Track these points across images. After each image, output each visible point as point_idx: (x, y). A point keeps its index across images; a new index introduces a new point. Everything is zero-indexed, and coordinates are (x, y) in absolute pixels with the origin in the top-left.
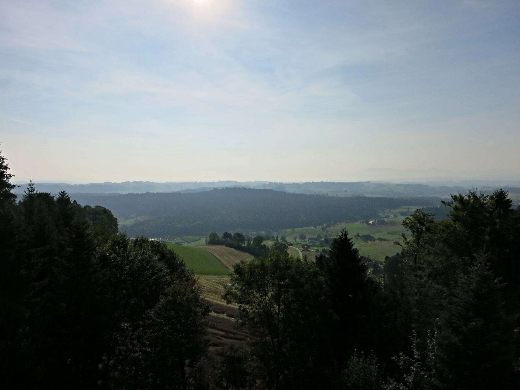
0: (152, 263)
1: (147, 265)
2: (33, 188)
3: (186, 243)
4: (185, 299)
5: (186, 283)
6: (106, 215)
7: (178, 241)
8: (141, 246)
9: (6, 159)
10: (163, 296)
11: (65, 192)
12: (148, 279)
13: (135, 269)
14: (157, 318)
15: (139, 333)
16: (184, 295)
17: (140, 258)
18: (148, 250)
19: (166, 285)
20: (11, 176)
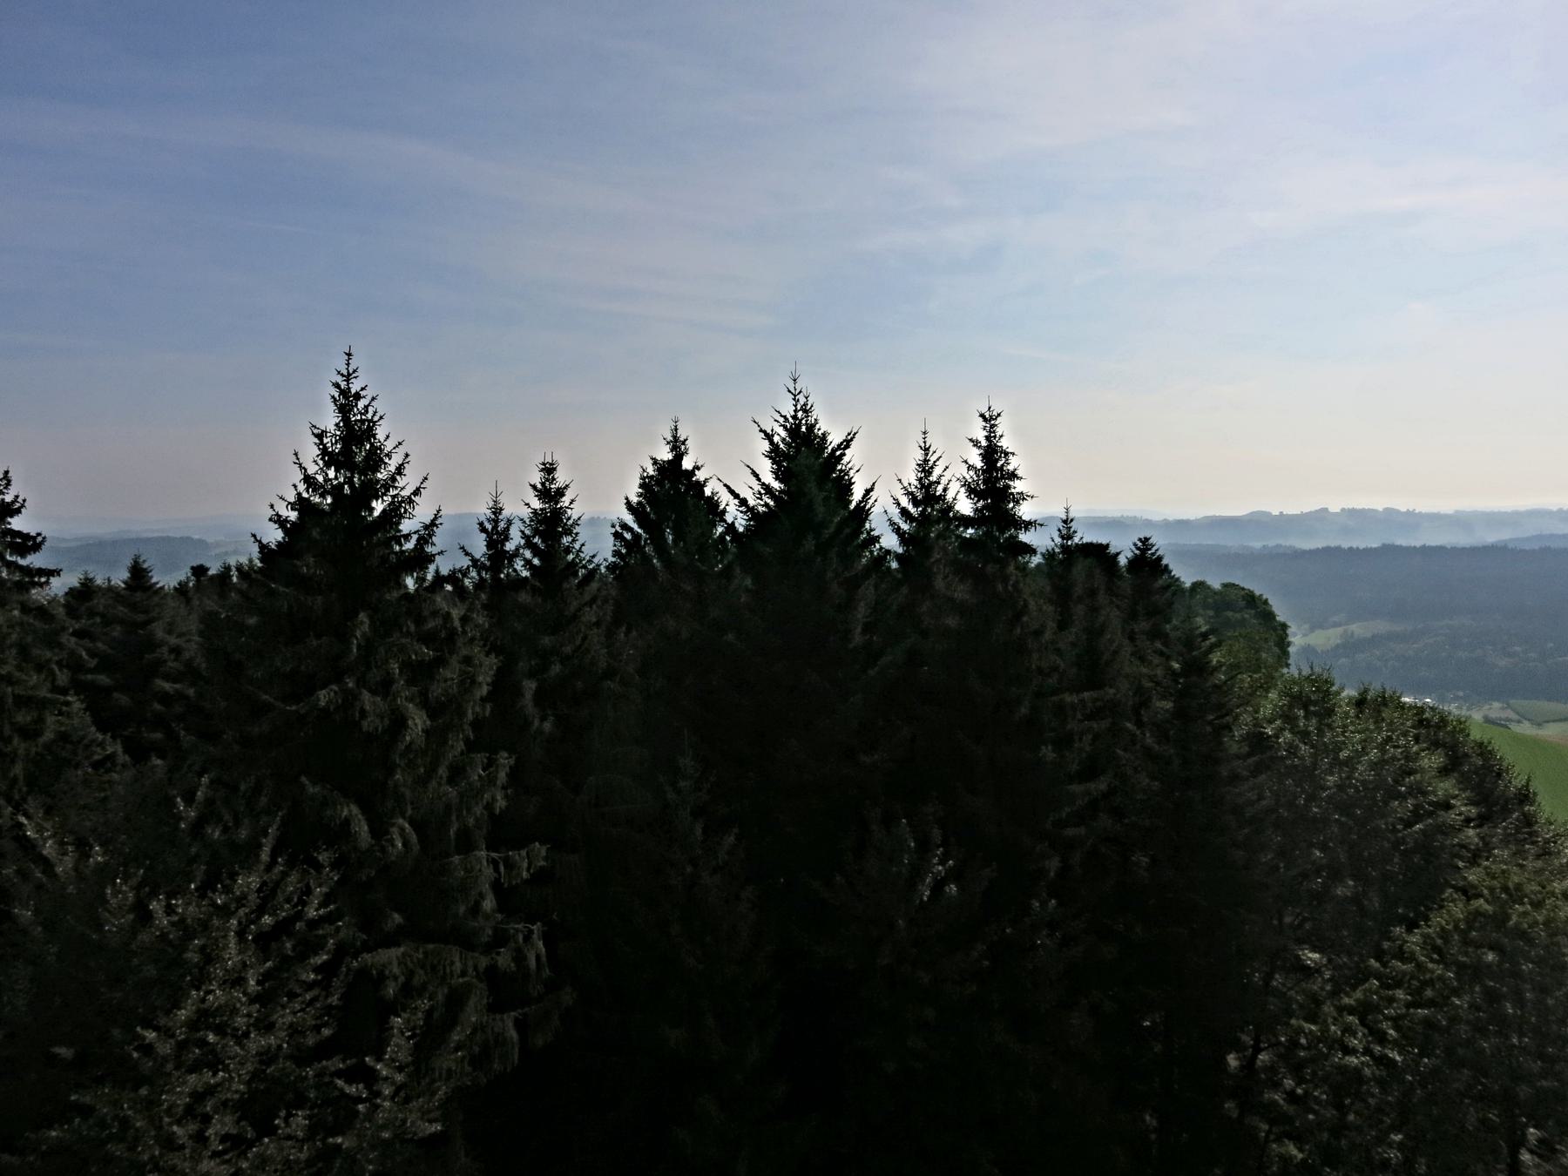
0: (1418, 776)
1: (1396, 782)
2: (1072, 530)
3: (1527, 724)
4: (1540, 919)
5: (1539, 864)
6: (1253, 612)
7: (1493, 715)
8: (1378, 720)
9: (1013, 454)
10: (1456, 893)
11: (1151, 541)
12: (1400, 827)
13: (1356, 788)
14: (1432, 961)
15: (1368, 994)
16: (1538, 905)
17: (1374, 754)
18: (1405, 734)
19: (1461, 858)
20: (1024, 499)
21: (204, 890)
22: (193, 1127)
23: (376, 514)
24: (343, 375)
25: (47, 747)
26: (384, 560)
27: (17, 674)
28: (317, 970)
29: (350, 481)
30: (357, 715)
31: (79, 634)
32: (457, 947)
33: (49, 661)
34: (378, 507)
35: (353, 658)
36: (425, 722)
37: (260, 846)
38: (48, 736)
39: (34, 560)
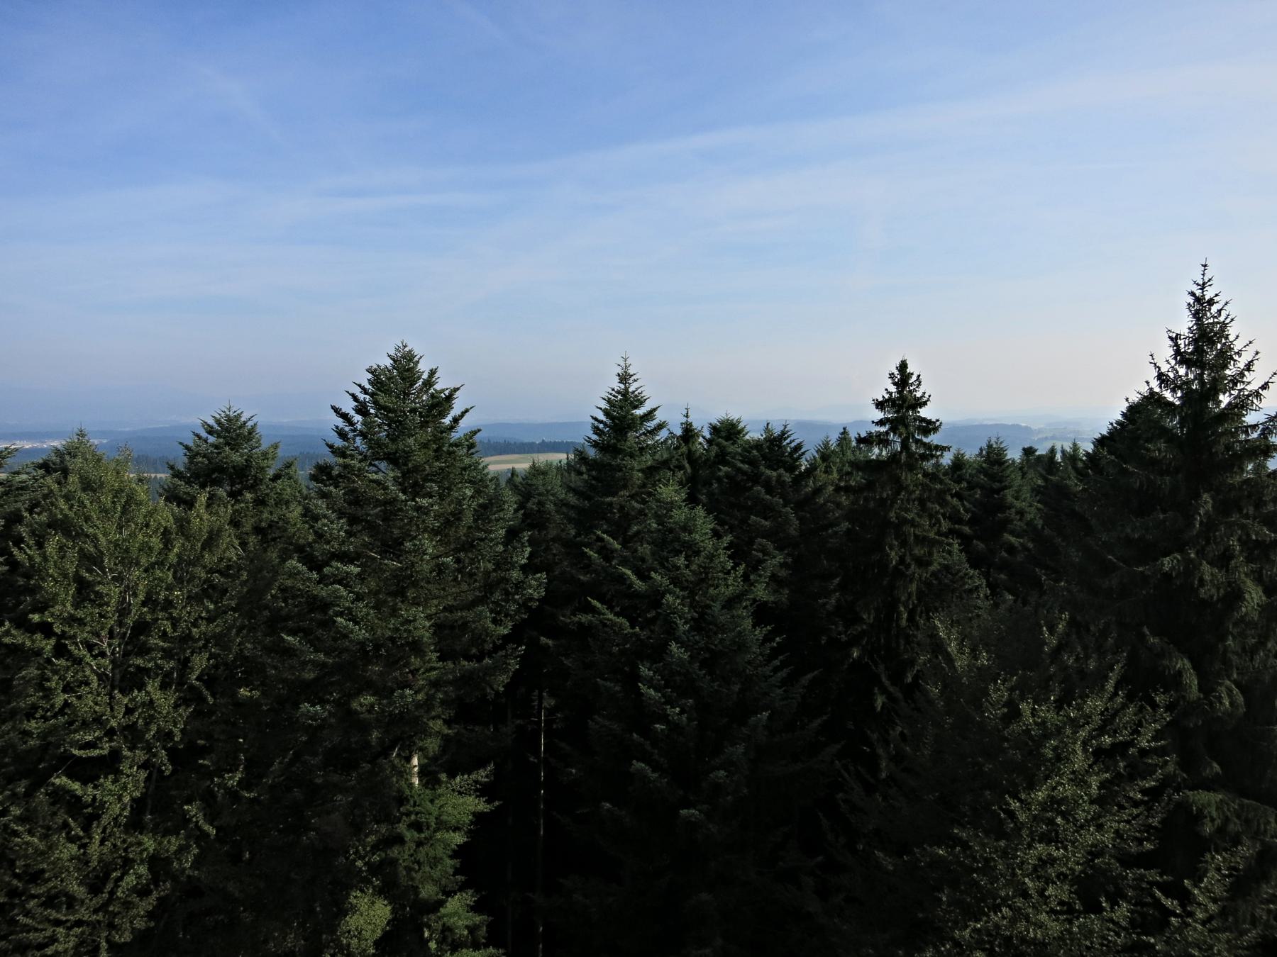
21: (1059, 706)
22: (1040, 884)
23: (1223, 406)
24: (1198, 285)
25: (934, 574)
26: (1228, 447)
27: (917, 519)
28: (1144, 792)
29: (1199, 377)
30: (1196, 582)
31: (958, 495)
32: (1273, 809)
33: (937, 512)
34: (1225, 399)
35: (1195, 533)
36: (1261, 597)
37: (1106, 678)
38: (935, 567)
39: (933, 439)
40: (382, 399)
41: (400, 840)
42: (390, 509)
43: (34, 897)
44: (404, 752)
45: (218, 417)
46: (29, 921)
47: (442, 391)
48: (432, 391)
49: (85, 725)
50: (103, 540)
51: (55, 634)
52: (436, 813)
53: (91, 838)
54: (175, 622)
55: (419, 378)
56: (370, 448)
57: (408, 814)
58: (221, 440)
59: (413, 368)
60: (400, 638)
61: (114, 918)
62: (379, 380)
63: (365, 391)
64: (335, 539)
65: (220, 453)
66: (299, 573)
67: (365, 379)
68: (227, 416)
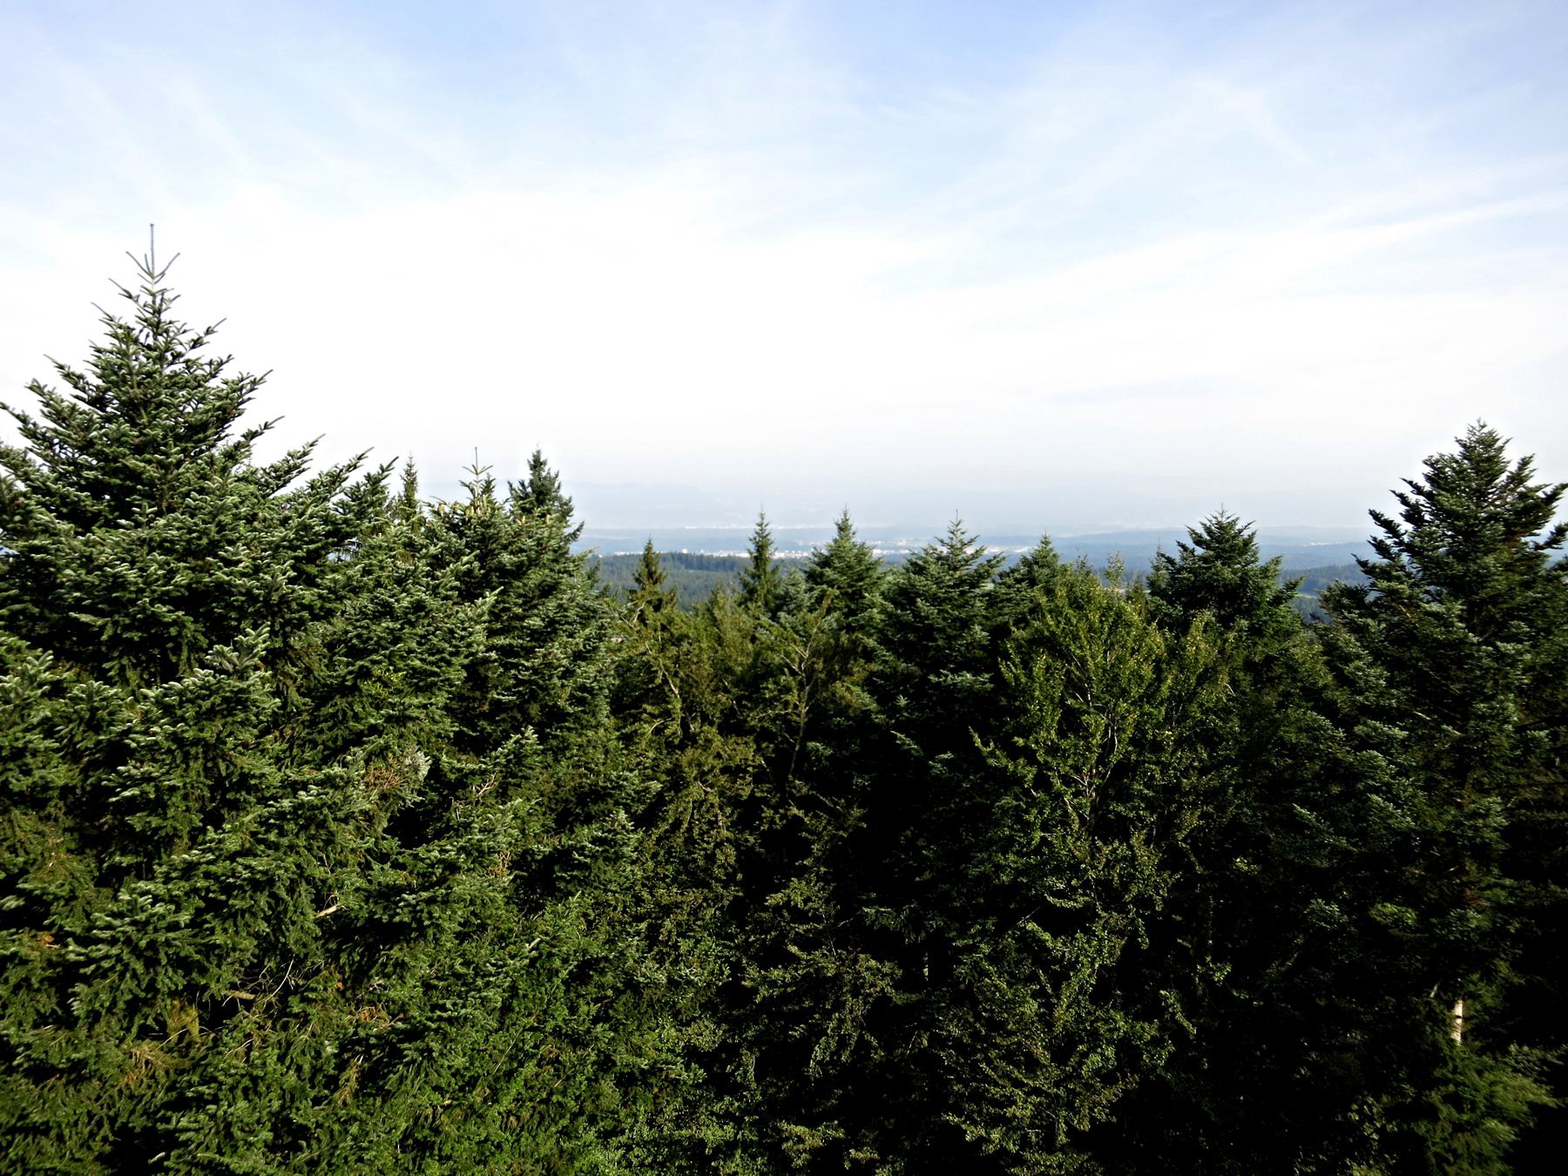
40: (1446, 500)
41: (1432, 1114)
42: (1451, 655)
43: (996, 1046)
44: (1446, 994)
45: (1208, 524)
46: (992, 1073)
47: (1539, 488)
48: (1521, 489)
49: (1058, 871)
50: (1091, 664)
51: (1037, 762)
52: (1485, 1091)
53: (1059, 999)
54: (1165, 767)
55: (1502, 471)
56: (1425, 569)
57: (1446, 1082)
58: (1212, 553)
59: (1494, 457)
60: (1461, 836)
61: (1074, 1097)
62: (1439, 475)
63: (1418, 490)
64: (1372, 688)
65: (1210, 568)
66: (1321, 727)
67: (1419, 474)
68: (1219, 523)
